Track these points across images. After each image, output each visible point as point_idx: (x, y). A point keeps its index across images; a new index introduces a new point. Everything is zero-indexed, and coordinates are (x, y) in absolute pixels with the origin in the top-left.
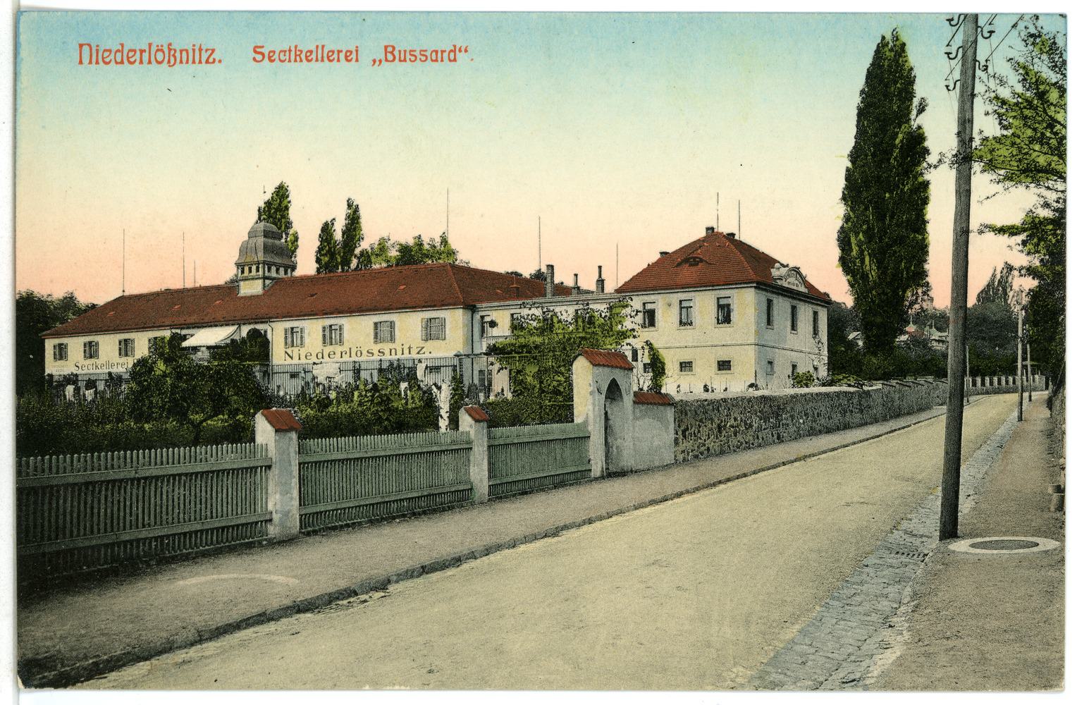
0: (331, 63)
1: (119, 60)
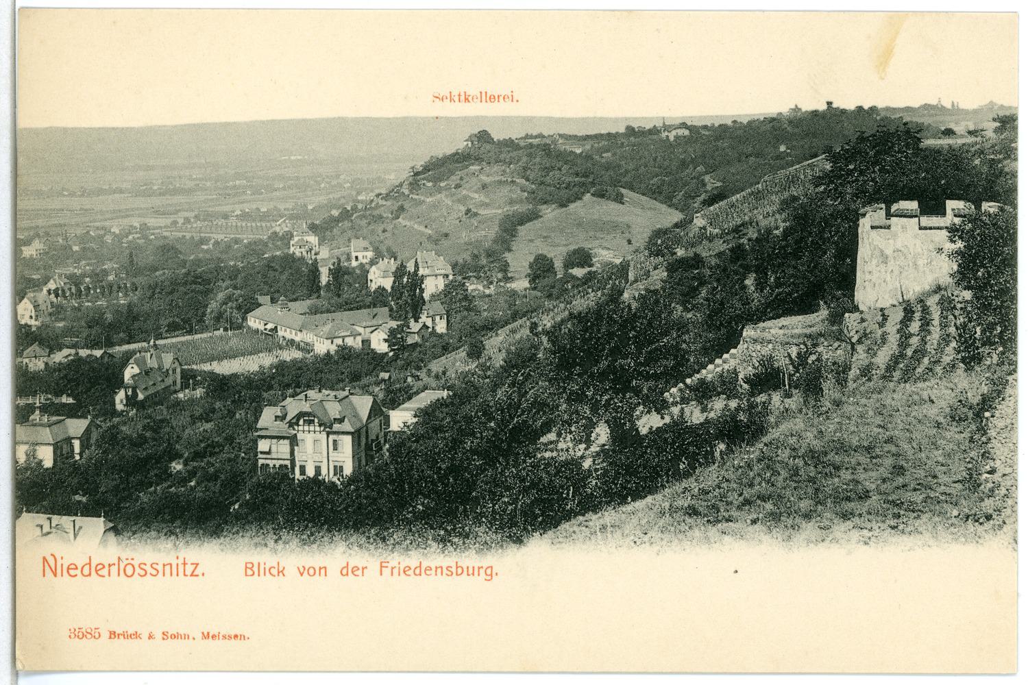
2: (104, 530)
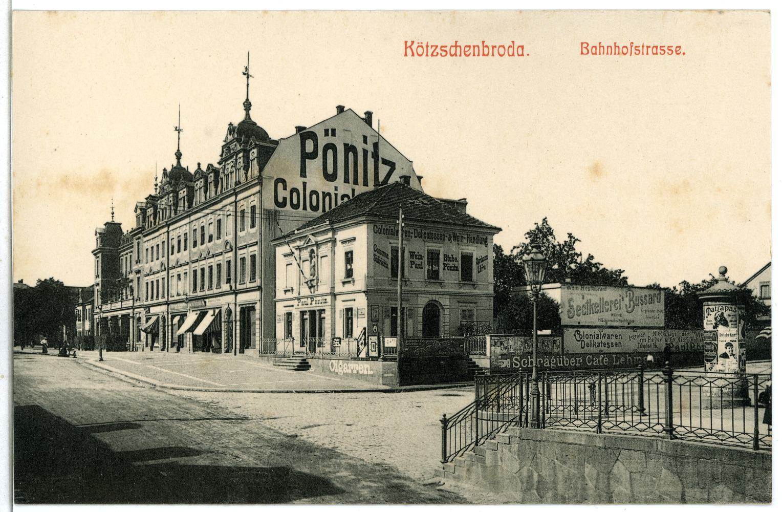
0: (467, 58)
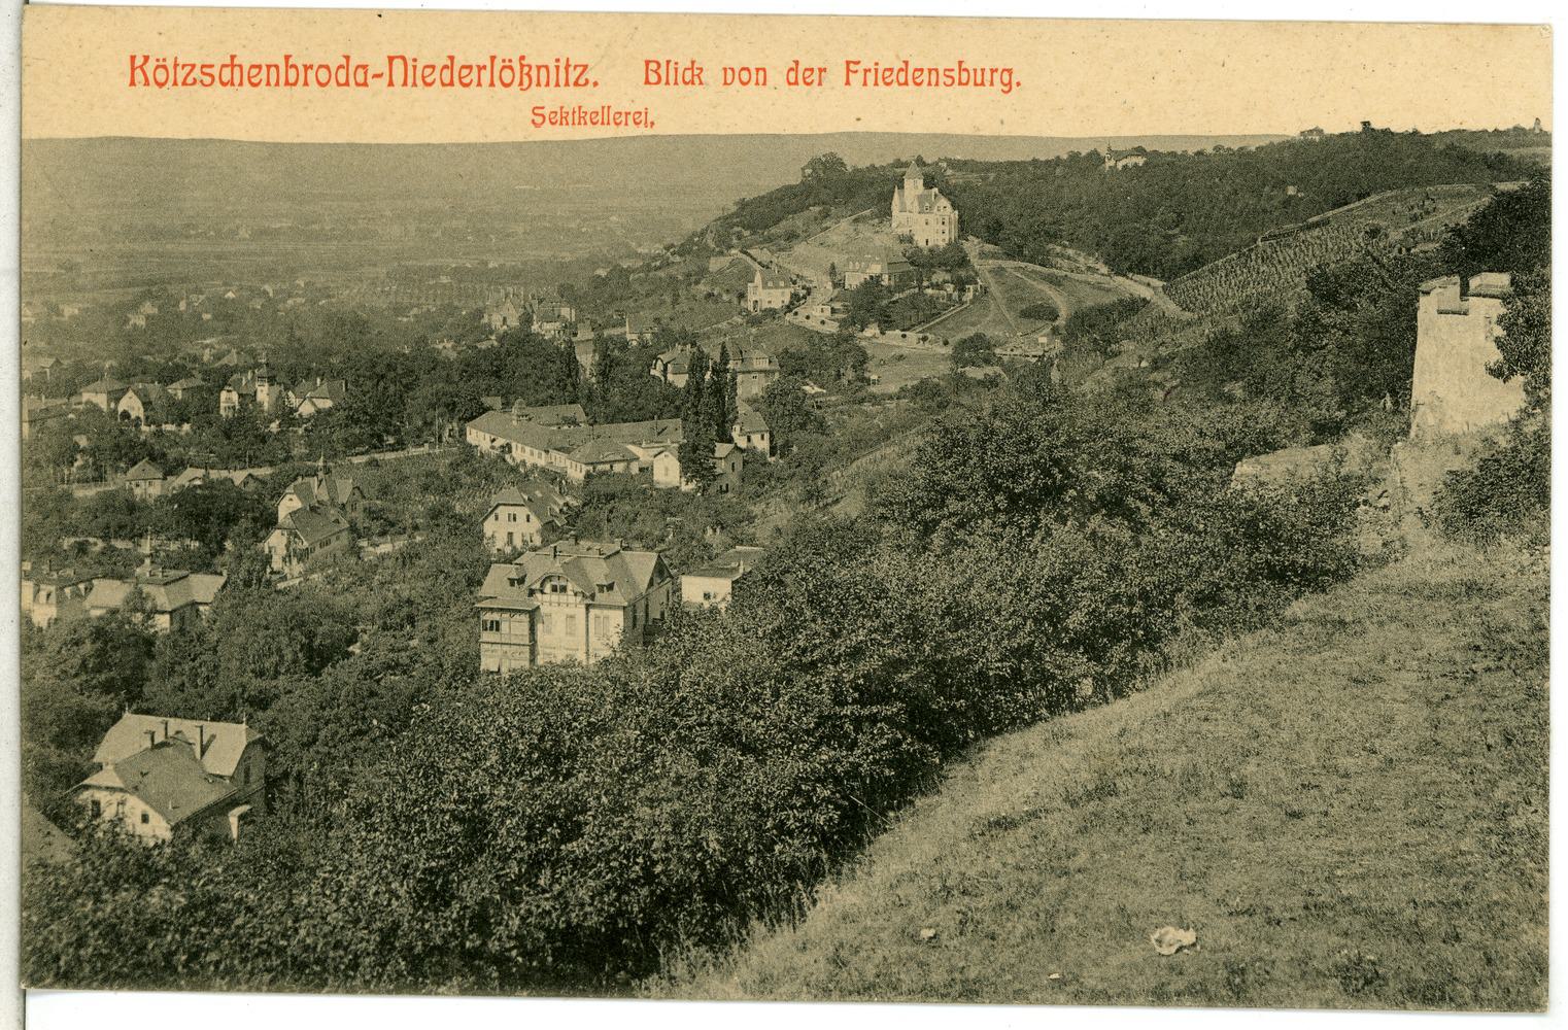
0: (256, 89)
1: (447, 80)
2: (245, 743)
